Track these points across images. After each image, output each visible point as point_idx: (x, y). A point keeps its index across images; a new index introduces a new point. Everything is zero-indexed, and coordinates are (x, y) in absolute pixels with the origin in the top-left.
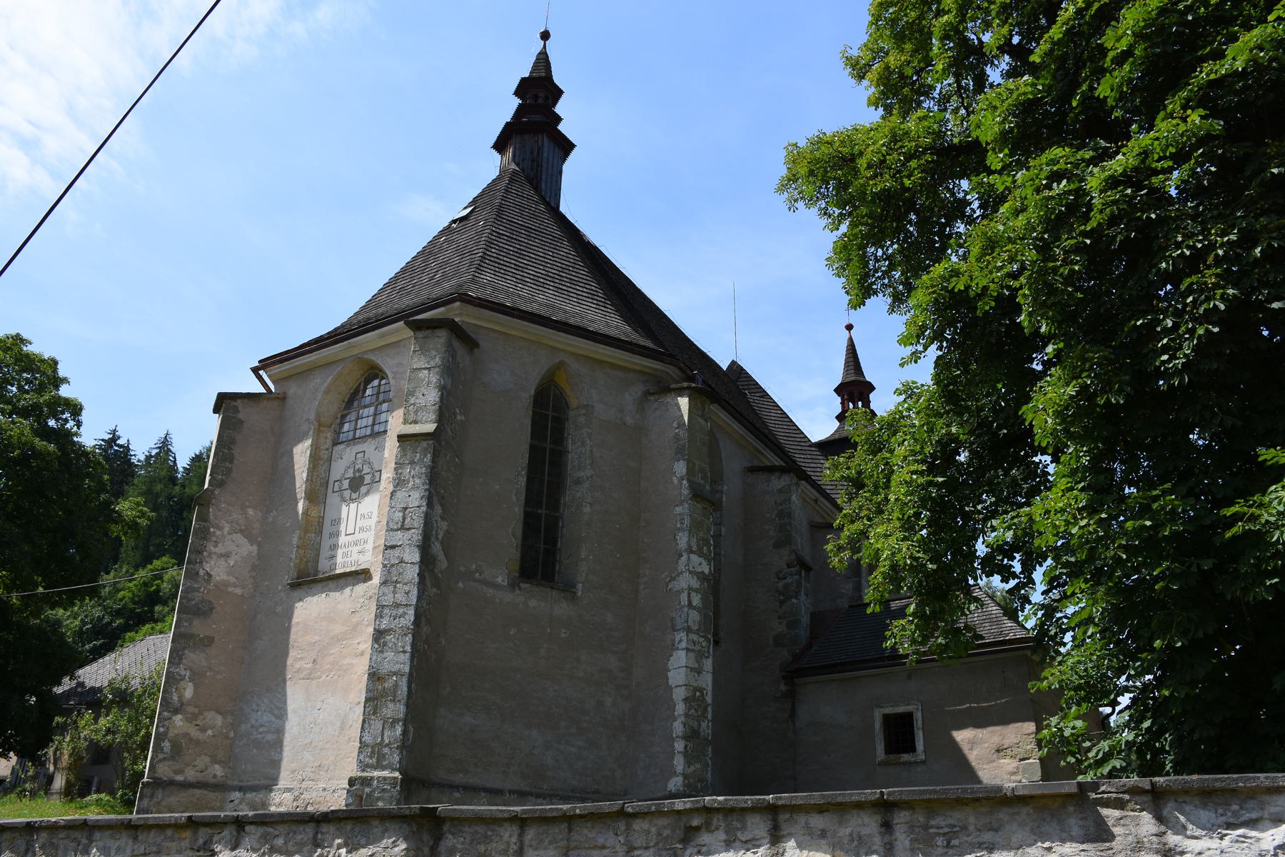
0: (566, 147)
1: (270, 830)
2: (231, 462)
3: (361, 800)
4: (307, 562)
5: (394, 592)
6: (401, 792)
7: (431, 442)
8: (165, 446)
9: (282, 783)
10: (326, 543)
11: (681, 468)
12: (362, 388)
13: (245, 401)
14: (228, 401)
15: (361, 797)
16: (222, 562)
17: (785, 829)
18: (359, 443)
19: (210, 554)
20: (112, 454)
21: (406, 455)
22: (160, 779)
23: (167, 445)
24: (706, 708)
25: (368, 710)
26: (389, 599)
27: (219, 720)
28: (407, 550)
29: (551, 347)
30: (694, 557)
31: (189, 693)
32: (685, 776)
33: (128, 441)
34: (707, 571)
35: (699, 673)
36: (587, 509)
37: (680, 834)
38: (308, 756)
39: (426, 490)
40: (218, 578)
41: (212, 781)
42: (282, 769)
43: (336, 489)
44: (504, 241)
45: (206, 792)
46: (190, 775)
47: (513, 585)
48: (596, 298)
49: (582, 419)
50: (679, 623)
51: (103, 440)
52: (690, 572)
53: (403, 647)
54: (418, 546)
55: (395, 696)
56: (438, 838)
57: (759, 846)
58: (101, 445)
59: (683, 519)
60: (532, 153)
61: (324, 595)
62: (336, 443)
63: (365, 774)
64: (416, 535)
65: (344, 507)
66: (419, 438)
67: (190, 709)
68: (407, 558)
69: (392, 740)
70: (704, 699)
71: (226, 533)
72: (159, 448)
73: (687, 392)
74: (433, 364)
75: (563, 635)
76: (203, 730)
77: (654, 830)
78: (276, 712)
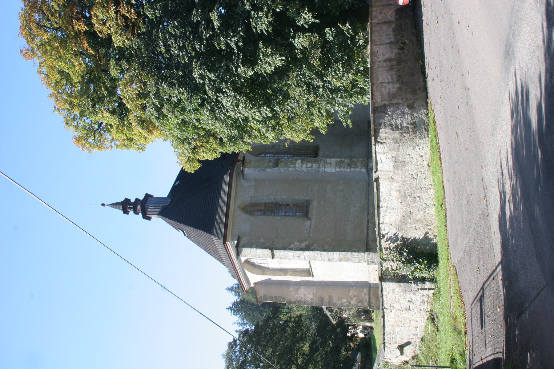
0: (148, 196)
2: (277, 297)
5: (318, 257)
8: (231, 289)
11: (268, 170)
13: (257, 295)
16: (307, 296)
19: (305, 299)
27: (351, 291)
30: (297, 166)
31: (345, 300)
32: (361, 168)
34: (300, 161)
35: (331, 164)
36: (284, 197)
41: (368, 291)
47: (310, 219)
49: (255, 199)
51: (231, 312)
52: (301, 167)
58: (233, 313)
67: (349, 299)
70: (339, 162)
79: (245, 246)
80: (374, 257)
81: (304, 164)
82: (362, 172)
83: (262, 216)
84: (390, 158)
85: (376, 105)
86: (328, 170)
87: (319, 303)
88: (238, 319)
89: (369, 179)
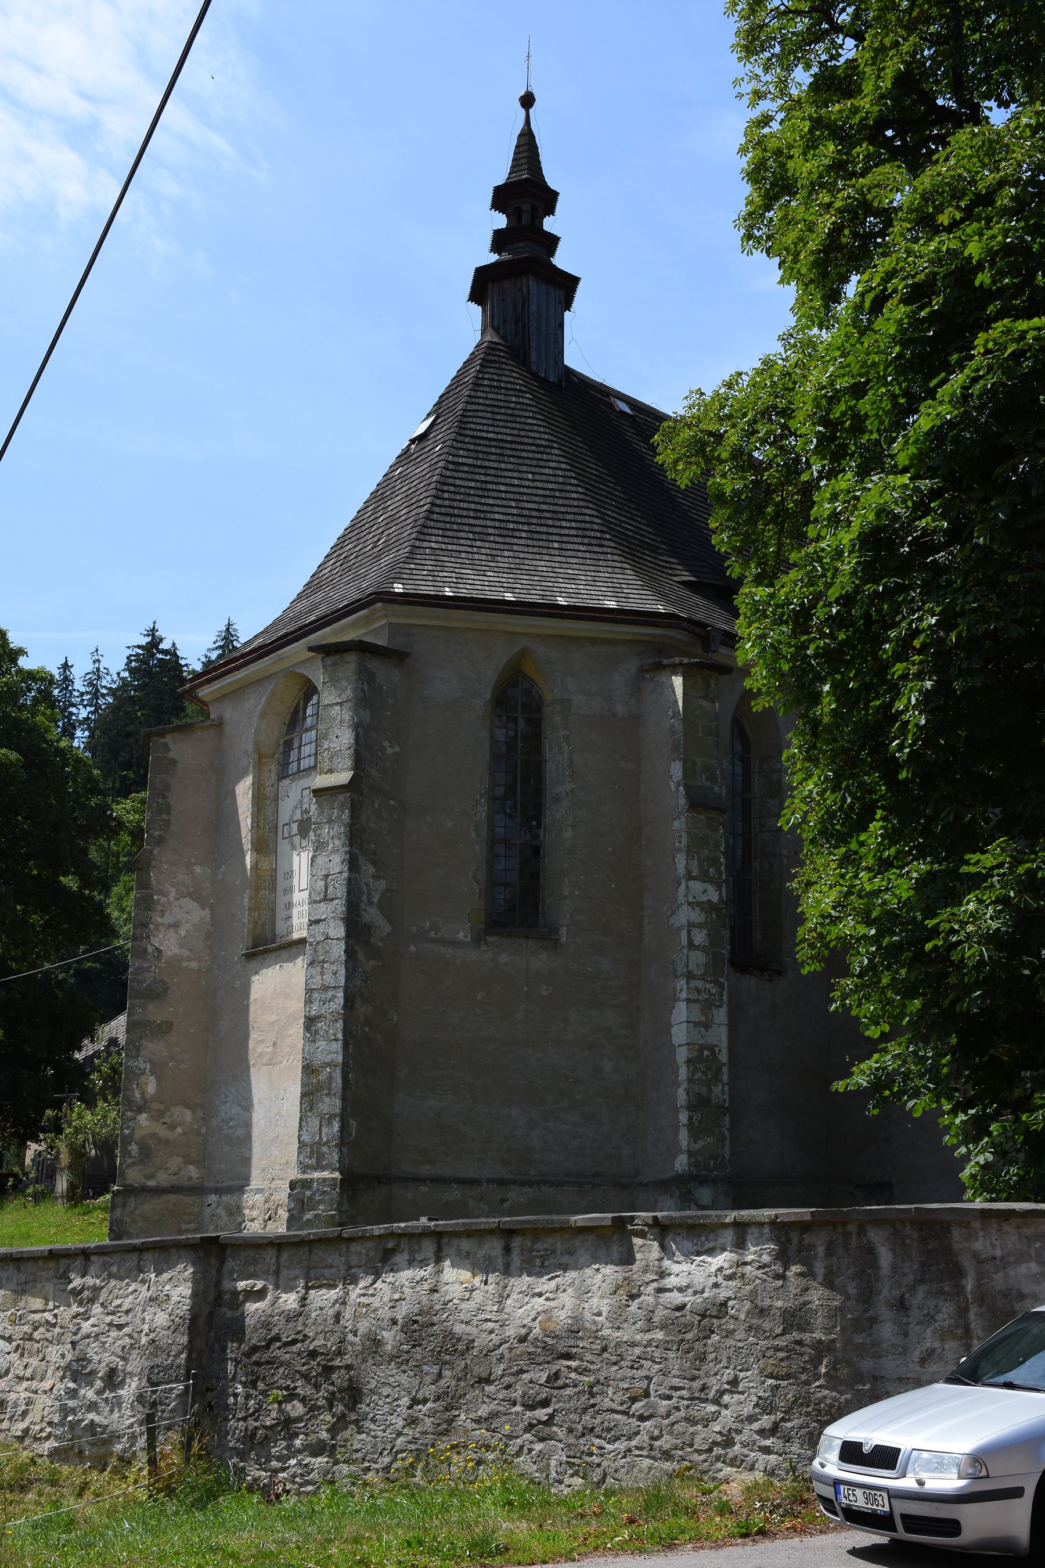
0: (568, 284)
1: (108, 1259)
2: (168, 813)
3: (303, 1204)
4: (264, 925)
5: (322, 973)
6: (341, 1194)
7: (348, 795)
9: (255, 1183)
10: (281, 901)
11: (677, 770)
12: (301, 706)
13: (176, 735)
14: (156, 739)
15: (303, 1201)
16: (171, 933)
17: (446, 1250)
18: (303, 777)
19: (157, 926)
20: (155, 666)
21: (323, 812)
22: (131, 1186)
23: (232, 641)
24: (719, 1070)
25: (304, 1106)
26: (317, 982)
27: (188, 1116)
28: (332, 924)
29: (508, 632)
30: (696, 886)
31: (151, 1088)
32: (690, 1154)
33: (174, 644)
34: (715, 898)
35: (707, 1026)
36: (568, 834)
37: (380, 1255)
38: (275, 1152)
39: (346, 853)
40: (169, 953)
42: (253, 1168)
43: (286, 835)
44: (464, 475)
45: (181, 1197)
46: (163, 1179)
47: (478, 940)
48: (589, 533)
49: (557, 718)
50: (681, 969)
51: (139, 647)
52: (690, 904)
53: (335, 1035)
54: (342, 919)
55: (329, 1090)
56: (222, 1262)
57: (428, 1265)
58: (137, 655)
59: (680, 836)
60: (515, 309)
61: (278, 966)
62: (283, 775)
63: (306, 1176)
64: (339, 906)
65: (295, 856)
66: (335, 791)
67: (155, 1106)
68: (332, 934)
69: (330, 1138)
71: (172, 899)
72: (220, 647)
73: (680, 669)
74: (344, 697)
75: (544, 993)
76: (172, 1128)
77: (363, 1251)
78: (243, 1103)
79: (365, 677)
80: (321, 1207)
81: (704, 915)
82: (675, 1157)
83: (487, 745)
84: (715, 1290)
85: (956, 1233)
86: (681, 1012)
87: (140, 982)
88: (113, 672)
89: (646, 1185)
